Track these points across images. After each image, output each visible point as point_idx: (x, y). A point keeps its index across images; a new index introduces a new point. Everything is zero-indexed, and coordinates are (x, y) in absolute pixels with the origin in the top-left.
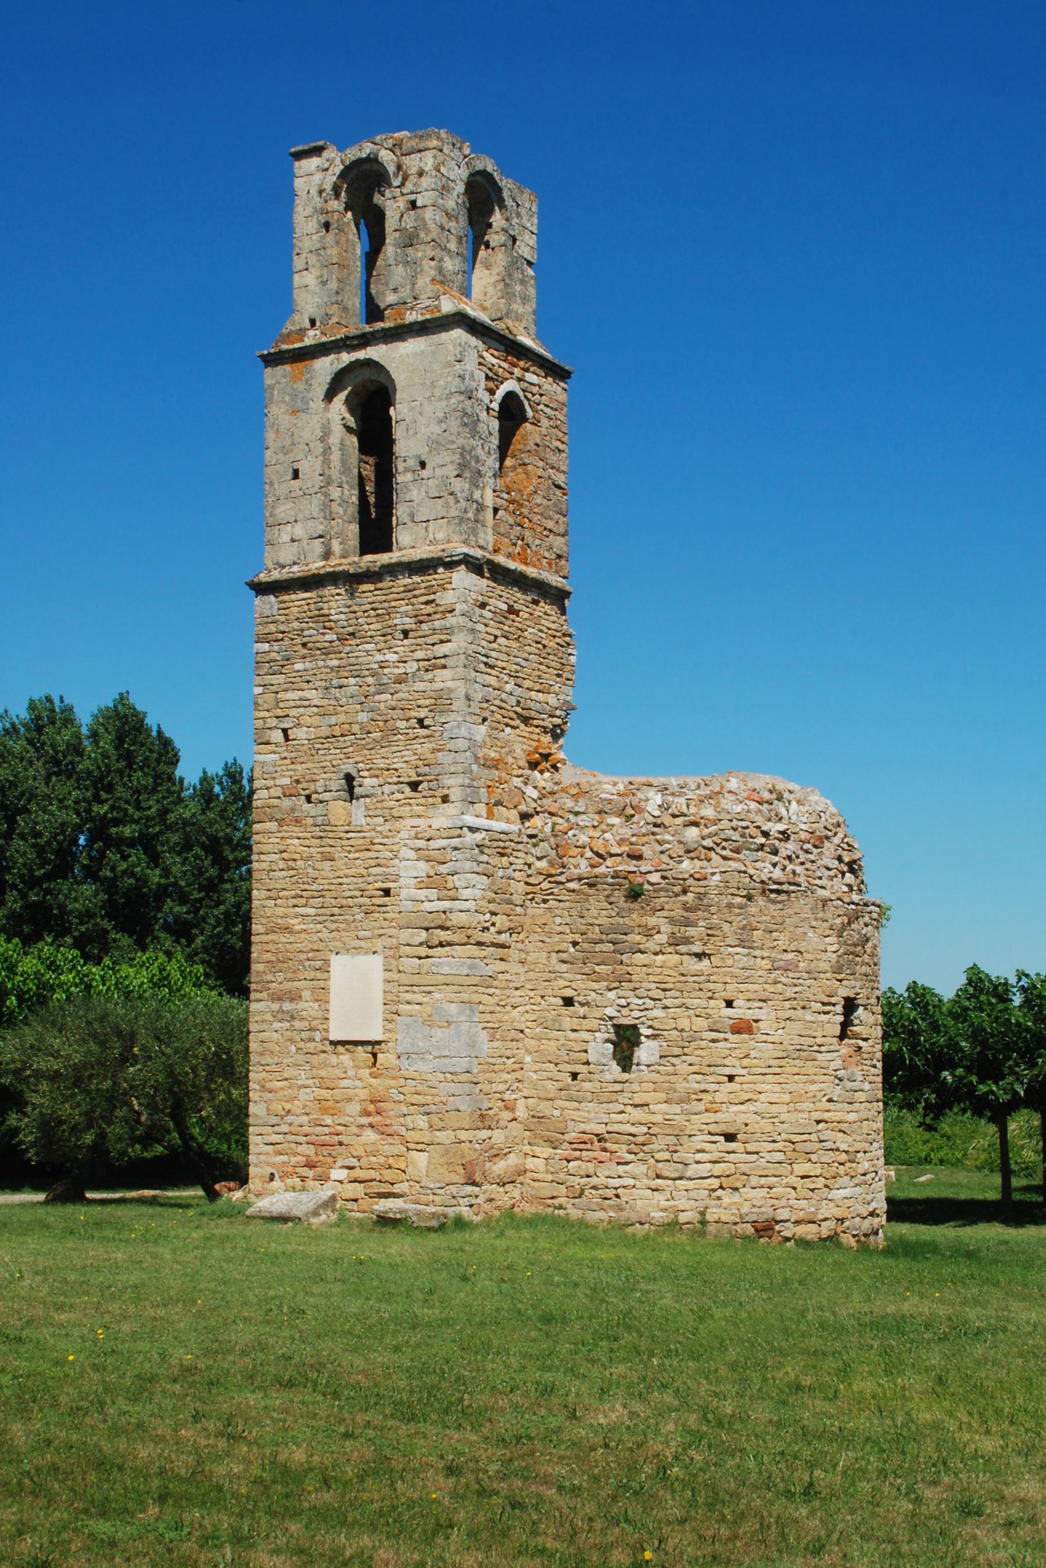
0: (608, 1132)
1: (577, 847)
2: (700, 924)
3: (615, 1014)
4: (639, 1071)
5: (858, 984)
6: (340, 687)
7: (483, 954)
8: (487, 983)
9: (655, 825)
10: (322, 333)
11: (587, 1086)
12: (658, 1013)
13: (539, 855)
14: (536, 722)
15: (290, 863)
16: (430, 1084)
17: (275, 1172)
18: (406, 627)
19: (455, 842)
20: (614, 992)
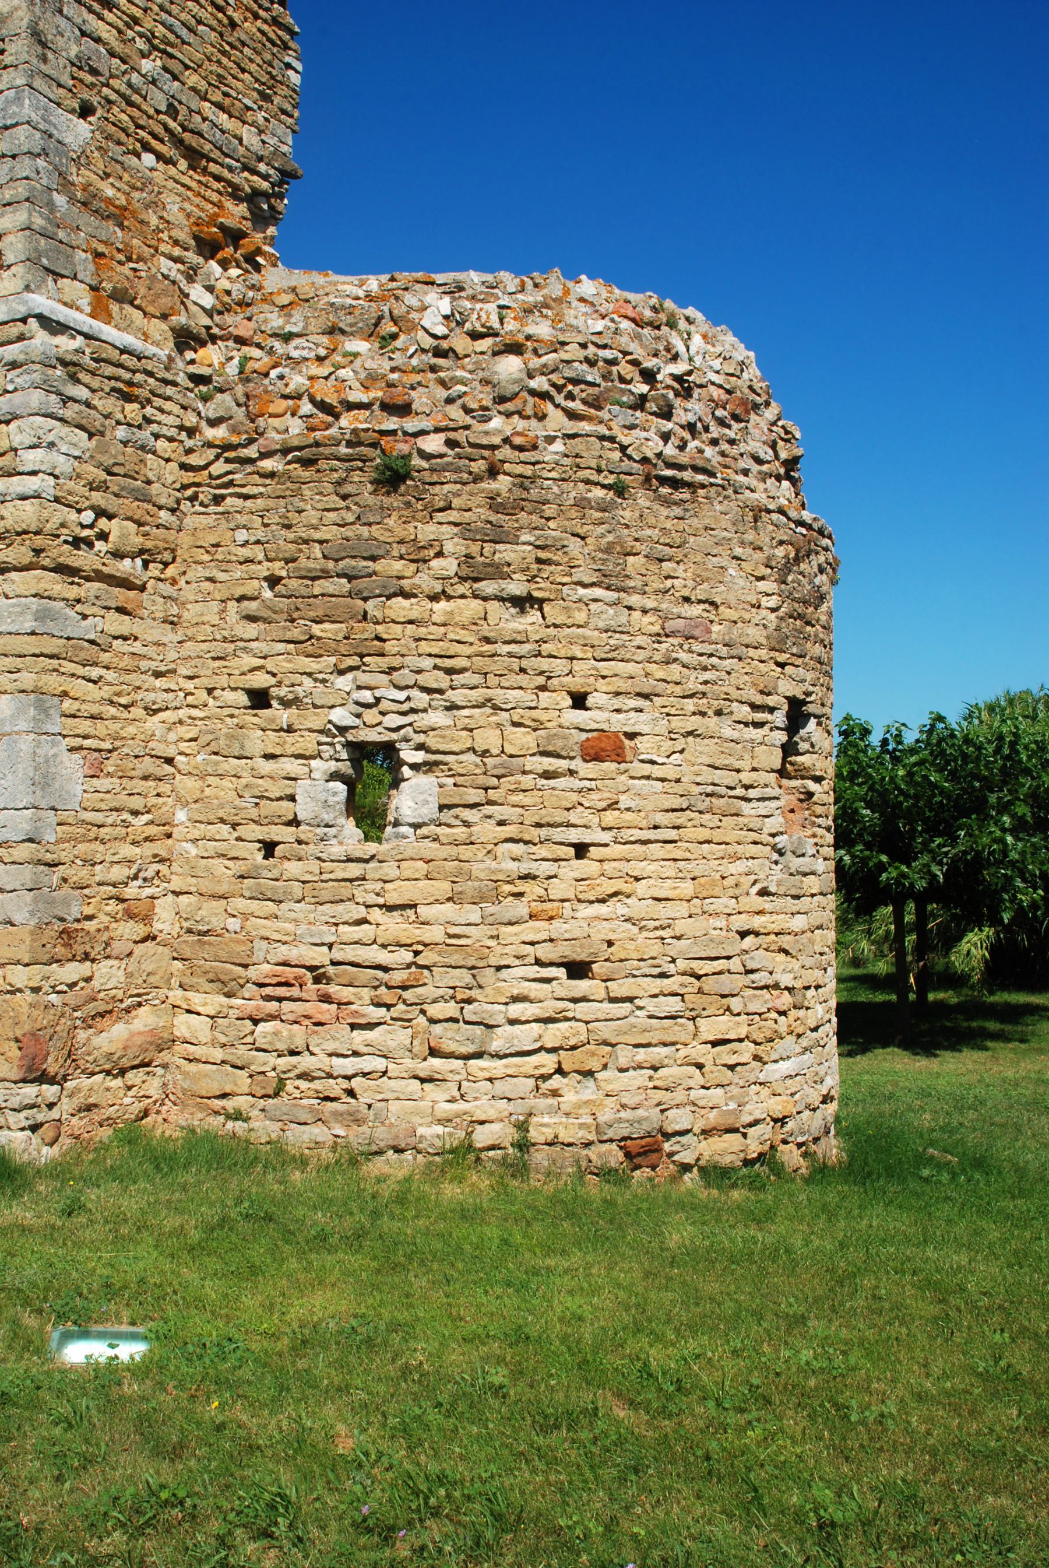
0: (334, 963)
1: (285, 397)
2: (524, 538)
3: (350, 721)
4: (397, 836)
5: (810, 676)
7: (73, 592)
8: (83, 655)
9: (439, 353)
11: (293, 868)
12: (437, 718)
13: (212, 415)
14: (213, 167)
20: (350, 676)
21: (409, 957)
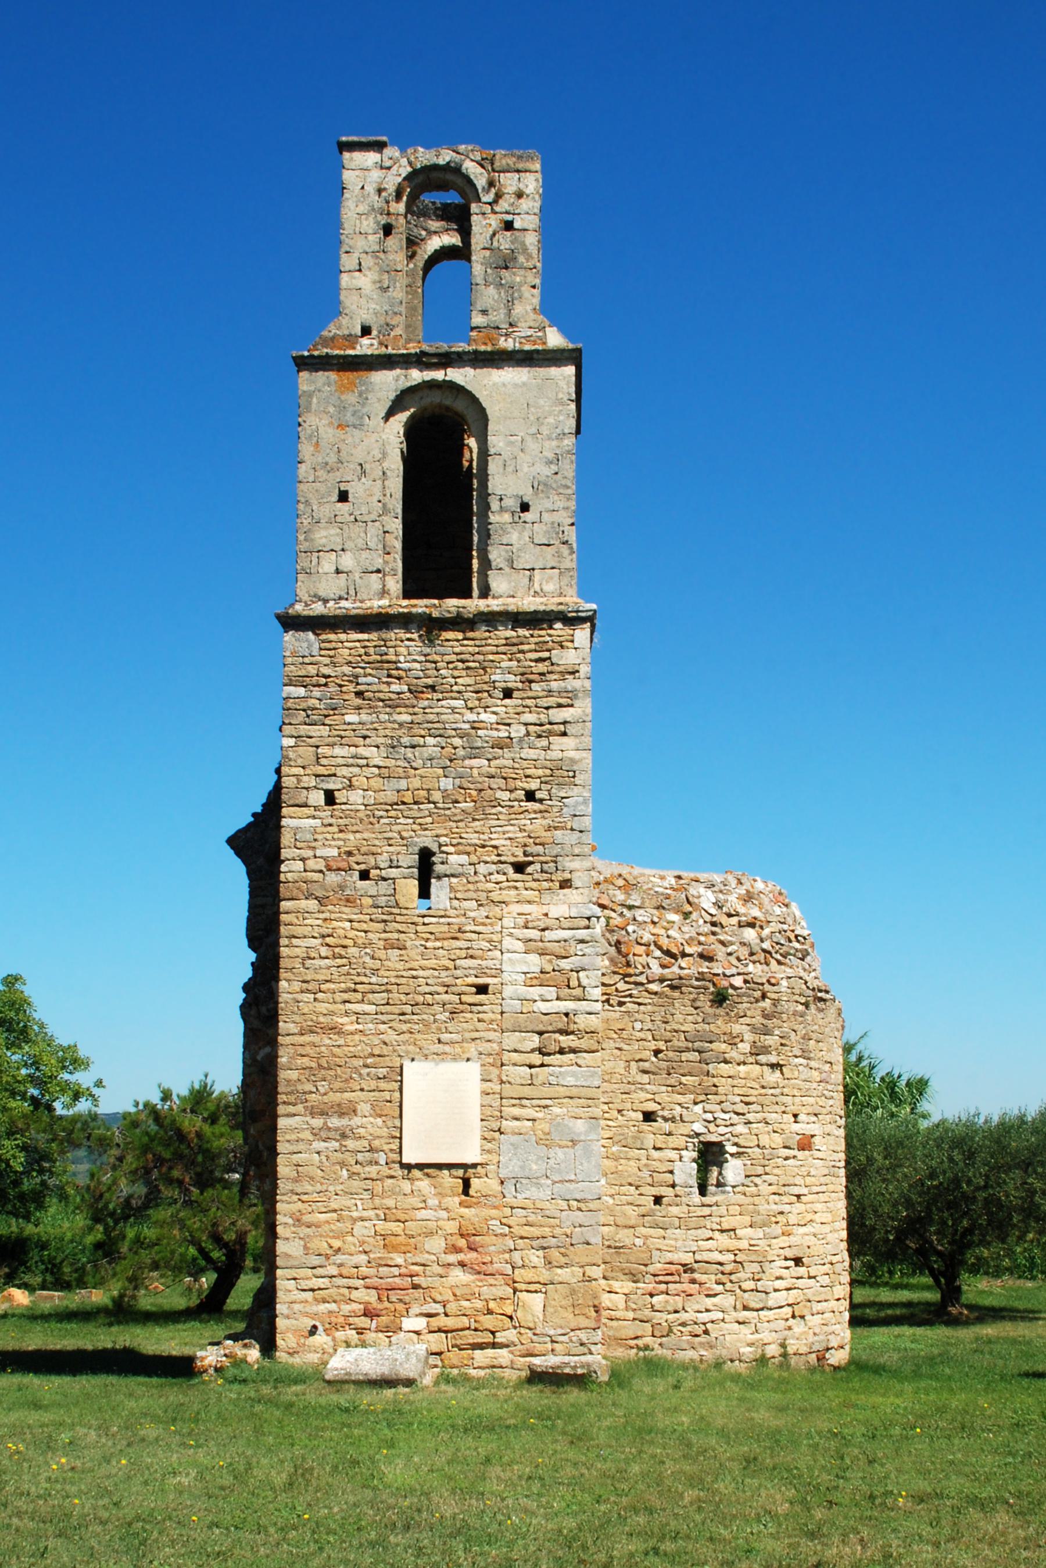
0: (696, 1262)
3: (703, 1130)
6: (413, 747)
10: (381, 344)
11: (674, 1210)
12: (740, 1129)
15: (337, 950)
16: (548, 1213)
17: (318, 1324)
18: (510, 685)
19: (582, 934)
20: (700, 1106)
21: (732, 1257)
